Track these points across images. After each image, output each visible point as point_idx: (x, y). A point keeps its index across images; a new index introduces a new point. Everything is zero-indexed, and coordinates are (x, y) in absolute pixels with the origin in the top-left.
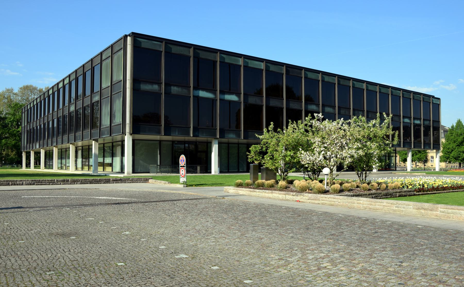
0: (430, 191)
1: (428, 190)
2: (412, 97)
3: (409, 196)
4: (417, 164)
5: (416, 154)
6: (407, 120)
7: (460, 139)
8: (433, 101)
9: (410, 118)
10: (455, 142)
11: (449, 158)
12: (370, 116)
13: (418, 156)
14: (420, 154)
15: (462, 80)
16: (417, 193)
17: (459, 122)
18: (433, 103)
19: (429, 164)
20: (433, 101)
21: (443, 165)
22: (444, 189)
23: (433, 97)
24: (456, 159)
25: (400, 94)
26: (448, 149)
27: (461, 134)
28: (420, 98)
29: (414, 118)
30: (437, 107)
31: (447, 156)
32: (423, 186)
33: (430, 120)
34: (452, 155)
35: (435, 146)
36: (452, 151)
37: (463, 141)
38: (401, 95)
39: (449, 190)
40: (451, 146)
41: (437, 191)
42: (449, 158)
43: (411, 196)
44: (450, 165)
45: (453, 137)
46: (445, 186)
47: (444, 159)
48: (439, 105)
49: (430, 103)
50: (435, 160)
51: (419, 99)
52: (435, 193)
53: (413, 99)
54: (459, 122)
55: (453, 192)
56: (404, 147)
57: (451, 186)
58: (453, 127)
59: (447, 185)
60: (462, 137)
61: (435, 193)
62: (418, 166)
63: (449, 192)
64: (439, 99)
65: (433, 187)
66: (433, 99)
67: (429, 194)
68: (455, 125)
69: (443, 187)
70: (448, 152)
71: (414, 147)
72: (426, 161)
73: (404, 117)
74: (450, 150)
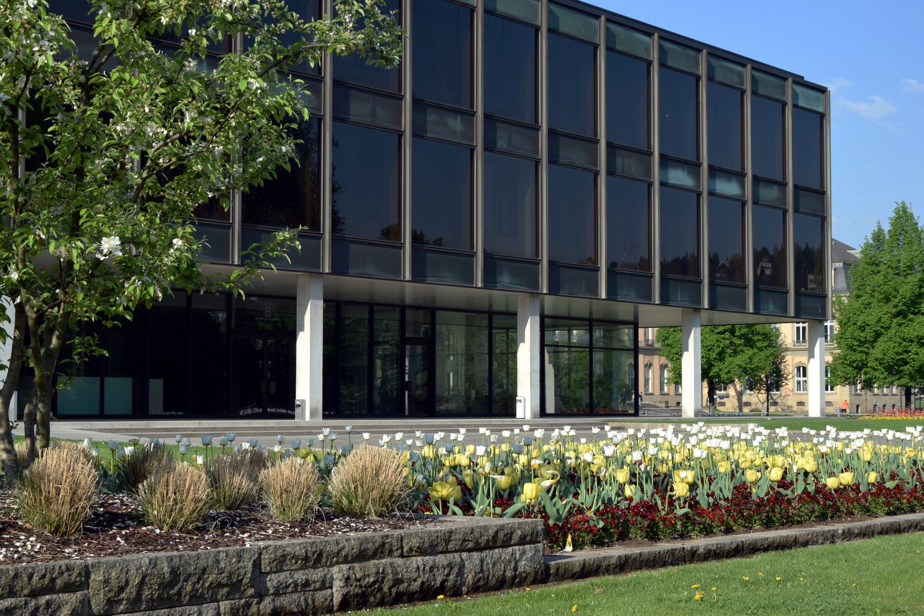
0: (708, 531)
1: (698, 517)
2: (703, 71)
3: (482, 587)
4: (745, 399)
5: (735, 352)
6: (679, 177)
7: (907, 287)
8: (795, 96)
9: (693, 167)
10: (887, 300)
11: (865, 365)
12: (502, 144)
13: (740, 359)
14: (751, 352)
15: (912, 82)
16: (589, 554)
17: (903, 218)
18: (795, 106)
19: (788, 392)
20: (795, 96)
21: (842, 394)
22: (827, 504)
23: (799, 81)
24: (894, 369)
25: (647, 49)
26: (862, 328)
27: (911, 267)
28: (741, 76)
29: (711, 168)
30: (815, 124)
31: (858, 356)
32: (663, 483)
33: (784, 185)
34: (876, 352)
35: (804, 301)
36: (878, 335)
37: (920, 295)
38: (655, 57)
39: (868, 512)
40: (871, 317)
41: (768, 524)
42: (865, 365)
43: (501, 584)
44: (869, 398)
45: (879, 278)
46: (831, 483)
47: (848, 370)
48: (821, 118)
49: (784, 104)
50: (810, 367)
51: (734, 81)
52: (753, 549)
53: (710, 79)
54: (903, 218)
55: (898, 530)
56: (665, 301)
57: (880, 486)
58: (878, 236)
59: (847, 478)
60: (914, 279)
61: (753, 549)
62: (748, 404)
63: (865, 534)
64: (823, 90)
65: (742, 491)
66: (799, 89)
67: (693, 556)
68: (887, 227)
69: (821, 490)
70: (862, 343)
71: (713, 306)
72: (775, 381)
73: (666, 161)
74: (868, 334)
